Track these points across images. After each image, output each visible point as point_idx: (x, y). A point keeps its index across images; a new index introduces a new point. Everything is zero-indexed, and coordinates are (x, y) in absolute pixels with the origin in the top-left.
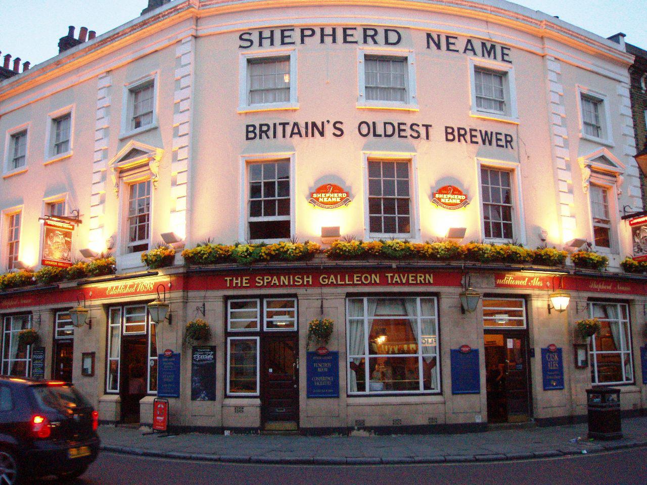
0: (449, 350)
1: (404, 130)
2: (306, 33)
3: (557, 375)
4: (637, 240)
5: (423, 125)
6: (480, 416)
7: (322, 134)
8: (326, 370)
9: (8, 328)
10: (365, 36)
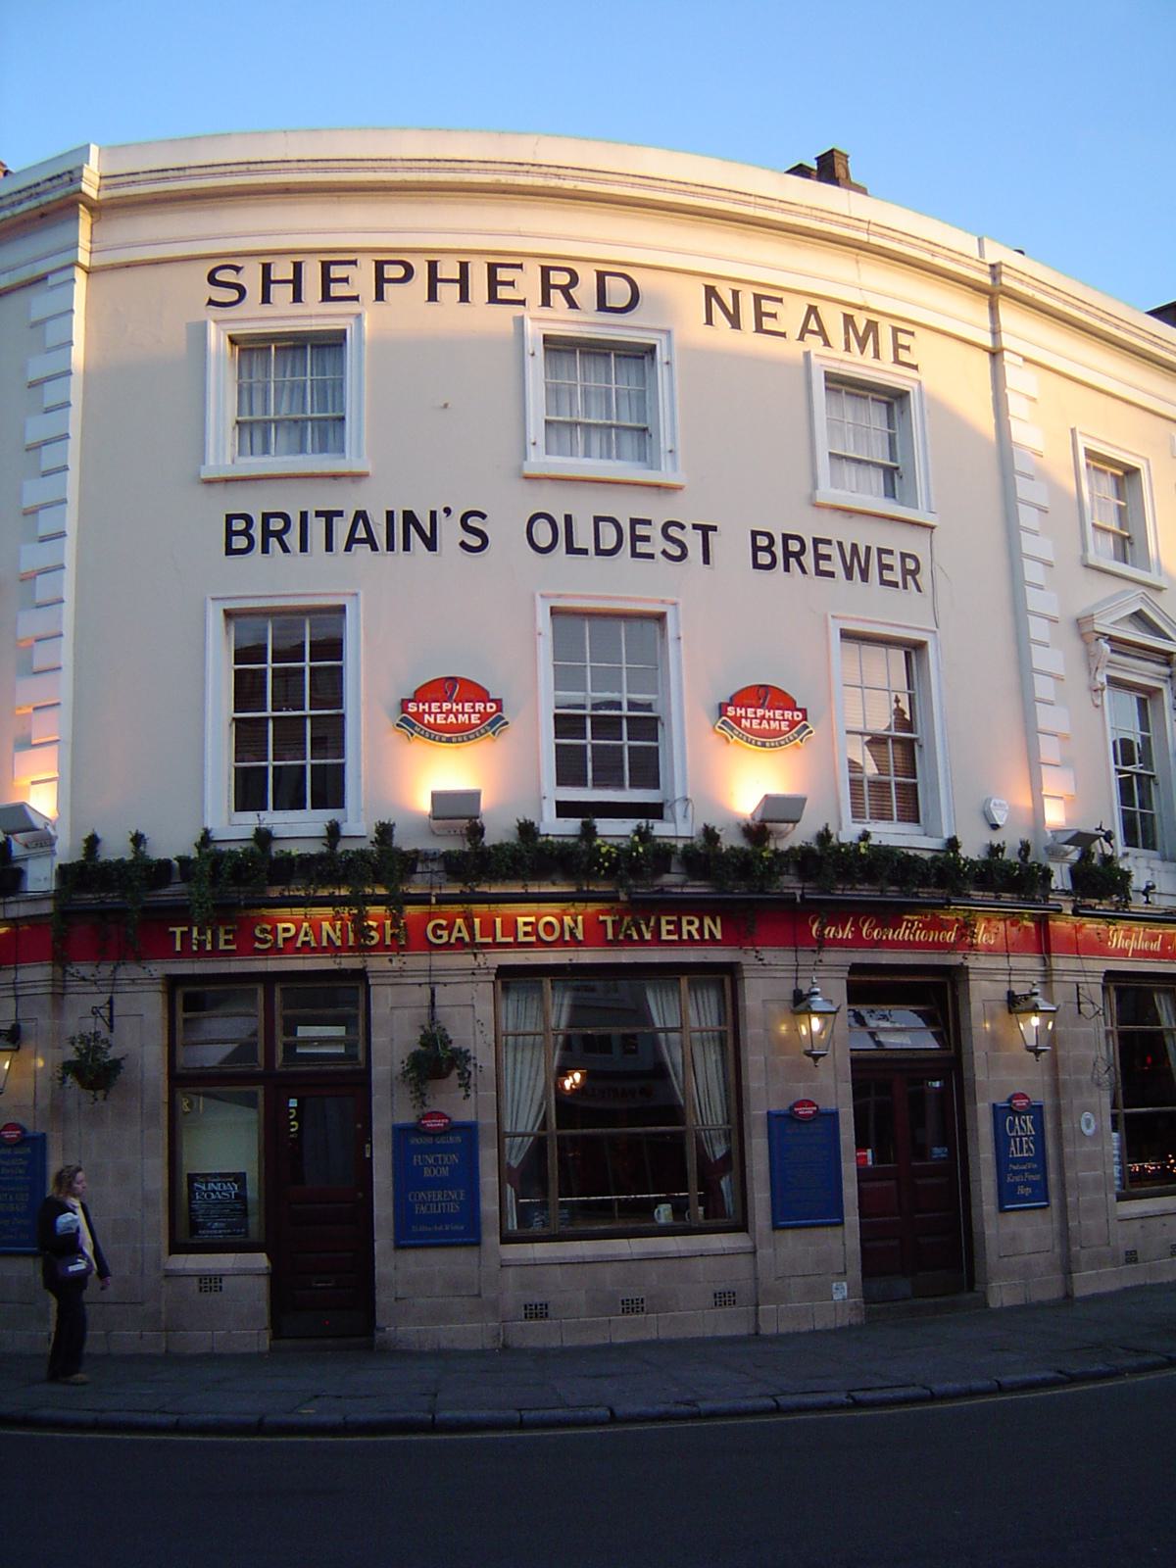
0: (765, 1112)
5: (695, 527)
6: (845, 1284)
7: (431, 544)
8: (445, 1171)
10: (546, 287)
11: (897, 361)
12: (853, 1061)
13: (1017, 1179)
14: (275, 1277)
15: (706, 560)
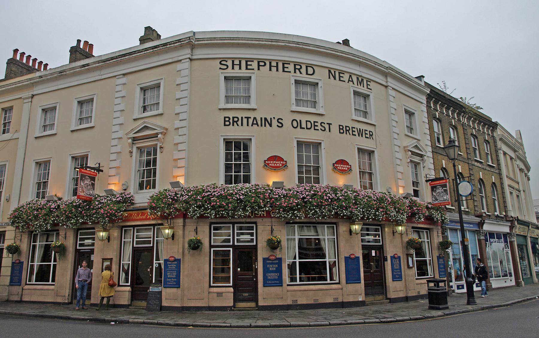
1: (317, 126)
2: (261, 63)
3: (399, 272)
4: (434, 194)
5: (327, 124)
7: (271, 125)
8: (275, 269)
9: (35, 241)
10: (295, 69)
11: (367, 88)
12: (90, 299)
13: (396, 273)
14: (234, 293)
15: (330, 131)
